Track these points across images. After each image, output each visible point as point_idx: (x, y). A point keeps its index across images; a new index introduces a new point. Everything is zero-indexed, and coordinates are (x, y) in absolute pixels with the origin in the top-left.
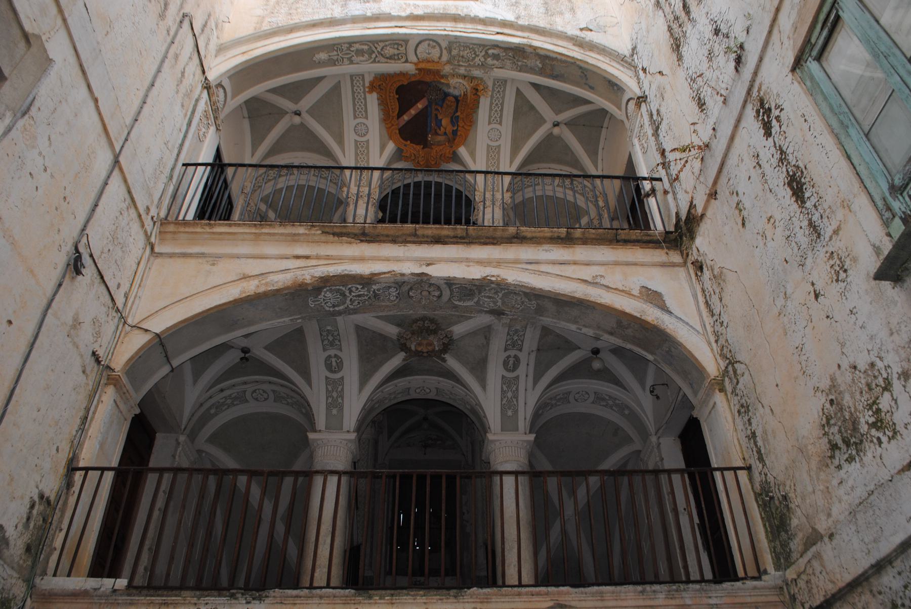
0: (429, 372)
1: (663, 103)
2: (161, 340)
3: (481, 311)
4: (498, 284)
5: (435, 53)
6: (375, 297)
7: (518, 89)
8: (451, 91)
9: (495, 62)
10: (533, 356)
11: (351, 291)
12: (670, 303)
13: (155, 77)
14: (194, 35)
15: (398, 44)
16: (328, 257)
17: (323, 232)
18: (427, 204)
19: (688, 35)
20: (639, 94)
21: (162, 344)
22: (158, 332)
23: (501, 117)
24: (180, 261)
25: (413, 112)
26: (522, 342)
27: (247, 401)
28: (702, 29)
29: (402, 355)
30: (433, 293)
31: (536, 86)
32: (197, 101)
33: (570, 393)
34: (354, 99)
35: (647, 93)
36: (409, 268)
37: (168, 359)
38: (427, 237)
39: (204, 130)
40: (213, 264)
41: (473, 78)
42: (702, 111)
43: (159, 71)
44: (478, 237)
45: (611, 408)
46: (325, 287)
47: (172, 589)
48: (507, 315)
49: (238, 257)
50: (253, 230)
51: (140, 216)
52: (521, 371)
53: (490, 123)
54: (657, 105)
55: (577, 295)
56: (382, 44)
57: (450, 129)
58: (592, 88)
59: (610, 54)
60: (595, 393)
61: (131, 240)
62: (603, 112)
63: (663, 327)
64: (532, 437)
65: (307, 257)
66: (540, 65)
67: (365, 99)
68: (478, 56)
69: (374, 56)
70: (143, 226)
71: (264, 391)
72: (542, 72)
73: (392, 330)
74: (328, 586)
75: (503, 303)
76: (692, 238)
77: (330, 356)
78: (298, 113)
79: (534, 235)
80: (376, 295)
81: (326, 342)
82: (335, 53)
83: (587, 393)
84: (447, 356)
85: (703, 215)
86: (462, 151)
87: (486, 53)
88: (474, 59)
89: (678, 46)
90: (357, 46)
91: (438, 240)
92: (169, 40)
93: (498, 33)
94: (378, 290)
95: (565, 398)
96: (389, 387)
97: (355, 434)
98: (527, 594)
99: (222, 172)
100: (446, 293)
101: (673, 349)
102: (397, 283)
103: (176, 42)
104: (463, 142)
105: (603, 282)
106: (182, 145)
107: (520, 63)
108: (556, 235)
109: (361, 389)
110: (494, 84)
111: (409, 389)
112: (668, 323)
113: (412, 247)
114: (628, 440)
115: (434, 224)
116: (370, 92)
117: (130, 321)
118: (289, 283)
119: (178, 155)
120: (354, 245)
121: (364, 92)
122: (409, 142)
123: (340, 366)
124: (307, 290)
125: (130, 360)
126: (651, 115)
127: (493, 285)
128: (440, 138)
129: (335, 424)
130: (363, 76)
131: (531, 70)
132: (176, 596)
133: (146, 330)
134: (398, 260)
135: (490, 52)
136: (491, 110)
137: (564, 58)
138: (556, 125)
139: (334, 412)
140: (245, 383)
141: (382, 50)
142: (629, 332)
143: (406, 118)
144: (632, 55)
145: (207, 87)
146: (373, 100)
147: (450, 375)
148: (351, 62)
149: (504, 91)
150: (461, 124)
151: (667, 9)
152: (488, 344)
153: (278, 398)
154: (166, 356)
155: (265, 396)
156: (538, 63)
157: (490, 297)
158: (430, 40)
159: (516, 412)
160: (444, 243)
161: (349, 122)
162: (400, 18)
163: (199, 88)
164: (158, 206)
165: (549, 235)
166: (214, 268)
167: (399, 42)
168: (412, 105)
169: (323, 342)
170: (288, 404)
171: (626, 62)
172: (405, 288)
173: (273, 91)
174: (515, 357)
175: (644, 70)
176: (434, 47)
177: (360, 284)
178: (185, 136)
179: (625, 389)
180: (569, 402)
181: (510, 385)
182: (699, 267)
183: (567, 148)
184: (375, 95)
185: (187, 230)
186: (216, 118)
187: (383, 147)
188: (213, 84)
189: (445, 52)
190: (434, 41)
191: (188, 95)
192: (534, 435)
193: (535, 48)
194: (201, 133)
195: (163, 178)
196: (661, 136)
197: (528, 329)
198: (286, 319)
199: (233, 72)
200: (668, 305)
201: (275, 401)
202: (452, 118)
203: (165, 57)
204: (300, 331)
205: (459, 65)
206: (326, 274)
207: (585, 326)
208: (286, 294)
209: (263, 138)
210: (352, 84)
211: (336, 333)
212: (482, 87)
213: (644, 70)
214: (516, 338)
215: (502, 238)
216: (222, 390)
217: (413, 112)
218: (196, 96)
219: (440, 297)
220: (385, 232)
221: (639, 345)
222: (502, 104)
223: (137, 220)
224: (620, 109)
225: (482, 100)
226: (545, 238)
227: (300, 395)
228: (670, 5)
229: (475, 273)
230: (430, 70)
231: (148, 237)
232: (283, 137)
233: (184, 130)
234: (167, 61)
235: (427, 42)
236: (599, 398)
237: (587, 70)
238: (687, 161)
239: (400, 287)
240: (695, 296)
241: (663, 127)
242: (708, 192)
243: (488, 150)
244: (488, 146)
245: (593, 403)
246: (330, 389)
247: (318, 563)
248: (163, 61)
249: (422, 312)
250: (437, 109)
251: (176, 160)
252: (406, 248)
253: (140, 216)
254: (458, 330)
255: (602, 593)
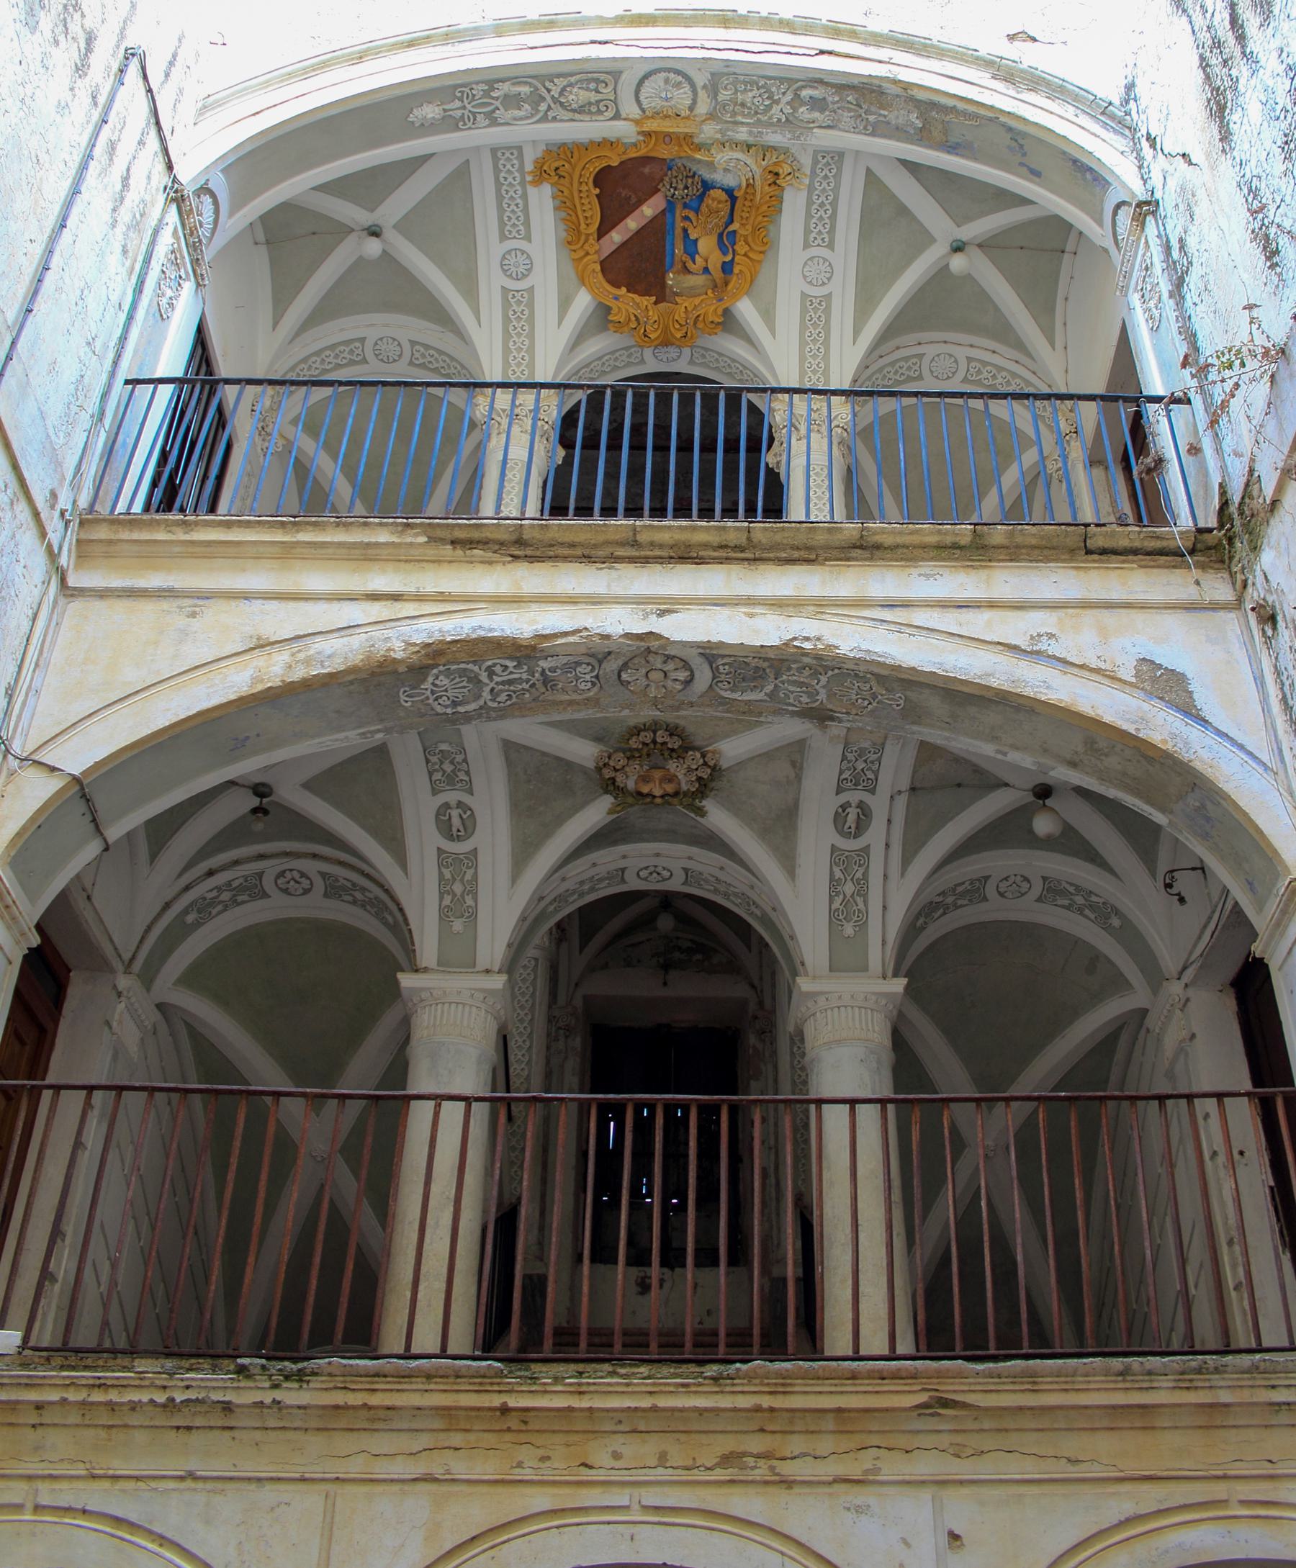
0: (671, 835)
1: (1193, 229)
2: (82, 788)
3: (778, 712)
4: (818, 658)
5: (682, 98)
6: (545, 683)
7: (868, 169)
8: (718, 177)
9: (816, 115)
10: (902, 802)
11: (491, 673)
12: (1204, 699)
13: (68, 205)
14: (150, 91)
15: (597, 81)
16: (442, 597)
17: (432, 539)
18: (666, 455)
19: (1241, 87)
20: (1141, 194)
21: (83, 795)
22: (77, 773)
23: (832, 232)
24: (121, 606)
25: (633, 223)
26: (876, 773)
27: (265, 895)
28: (1270, 82)
29: (607, 801)
30: (673, 675)
31: (912, 167)
32: (156, 232)
33: (987, 878)
34: (499, 198)
35: (1158, 195)
36: (618, 622)
37: (97, 827)
38: (661, 546)
39: (169, 293)
40: (193, 615)
41: (767, 149)
42: (1272, 267)
43: (75, 191)
44: (773, 547)
45: (1080, 911)
46: (437, 666)
47: (114, 1352)
48: (840, 721)
49: (246, 596)
50: (279, 537)
51: (36, 514)
52: (875, 835)
53: (806, 245)
54: (1179, 229)
55: (994, 682)
56: (561, 82)
57: (716, 259)
58: (1035, 174)
59: (1076, 98)
60: (1044, 879)
61: (19, 569)
62: (1061, 226)
63: (1185, 756)
64: (899, 985)
65: (396, 597)
66: (919, 124)
67: (525, 196)
68: (777, 102)
69: (543, 107)
70: (43, 534)
71: (303, 875)
72: (922, 136)
73: (584, 752)
74: (443, 1354)
75: (831, 695)
76: (1255, 548)
77: (447, 806)
78: (375, 232)
79: (899, 540)
80: (546, 681)
81: (437, 776)
82: (458, 104)
83: (1026, 879)
84: (708, 804)
85: (1275, 503)
86: (745, 309)
87: (797, 95)
88: (769, 108)
89: (1222, 108)
90: (506, 88)
91: (685, 556)
92: (96, 115)
93: (822, 52)
94: (553, 670)
95: (976, 890)
96: (580, 868)
97: (504, 977)
98: (870, 1375)
99: (212, 393)
100: (703, 677)
101: (1209, 806)
102: (592, 655)
103: (112, 117)
104: (749, 288)
105: (1054, 649)
106: (124, 338)
107: (871, 118)
108: (949, 540)
109: (515, 878)
110: (815, 162)
111: (623, 870)
112: (1198, 748)
113: (627, 570)
114: (1118, 983)
115: (675, 517)
116: (538, 181)
117: (16, 747)
118: (357, 659)
119: (116, 363)
120: (499, 567)
121: (523, 183)
122: (624, 290)
123: (469, 826)
124: (395, 672)
125: (18, 835)
126: (1167, 248)
127: (807, 660)
128: (698, 280)
129: (459, 956)
130: (520, 149)
131: (898, 133)
132: (124, 1369)
133: (53, 769)
134: (595, 601)
135: (805, 93)
136: (809, 216)
137: (971, 108)
138: (958, 248)
139: (458, 925)
140: (261, 857)
141: (561, 94)
142: (1113, 762)
143: (616, 237)
144: (1127, 102)
145: (177, 198)
146: (542, 200)
147: (713, 842)
148: (494, 122)
149: (838, 176)
150: (741, 247)
151: (1198, 20)
152: (799, 778)
153: (334, 890)
154: (94, 820)
155: (306, 883)
156: (913, 117)
157: (801, 684)
158: (669, 70)
159: (863, 926)
160: (700, 561)
161: (490, 249)
162: (603, 22)
163: (161, 198)
164: (76, 486)
165: (932, 539)
166: (195, 624)
167: (601, 77)
168: (629, 208)
169: (430, 774)
170: (355, 902)
171: (1112, 117)
172: (612, 666)
173: (323, 188)
174: (861, 805)
175: (1152, 141)
176: (678, 85)
177: (511, 658)
178: (130, 318)
179: (1112, 871)
180: (985, 899)
181: (848, 866)
182: (1269, 618)
183: (983, 298)
184: (547, 189)
185: (136, 536)
186: (196, 262)
187: (565, 303)
188: (189, 190)
189: (702, 94)
190: (678, 72)
191: (135, 226)
192: (904, 981)
193: (907, 86)
194: (164, 301)
195: (85, 420)
196: (1189, 303)
197: (888, 747)
198: (352, 734)
199: (232, 159)
200: (1198, 704)
201: (326, 895)
202: (721, 235)
203: (88, 157)
204: (381, 752)
205: (736, 123)
206: (437, 636)
207: (1015, 747)
208: (351, 683)
209: (299, 288)
210: (496, 167)
211: (459, 758)
212: (787, 169)
213: (1152, 141)
214: (860, 765)
215: (827, 548)
216: (211, 873)
217: (633, 223)
218: (154, 223)
219: (688, 682)
220: (568, 537)
221: (1137, 793)
222: (834, 204)
223: (32, 524)
224: (1100, 223)
225: (788, 195)
226: (924, 547)
227: (381, 886)
228: (1204, 10)
229: (767, 631)
230: (668, 135)
231: (52, 555)
232: (341, 281)
233: (126, 307)
234: (92, 164)
235: (663, 75)
236: (1053, 890)
237: (1025, 135)
238: (1237, 385)
239: (600, 662)
240: (1259, 680)
241: (1193, 280)
242: (1280, 465)
243: (804, 310)
244: (804, 296)
245: (1039, 900)
246: (448, 875)
247: (424, 1269)
248: (83, 167)
249: (648, 714)
250: (686, 218)
251: (113, 374)
252: (614, 574)
253: (36, 514)
254: (732, 749)
255: (1033, 1374)
